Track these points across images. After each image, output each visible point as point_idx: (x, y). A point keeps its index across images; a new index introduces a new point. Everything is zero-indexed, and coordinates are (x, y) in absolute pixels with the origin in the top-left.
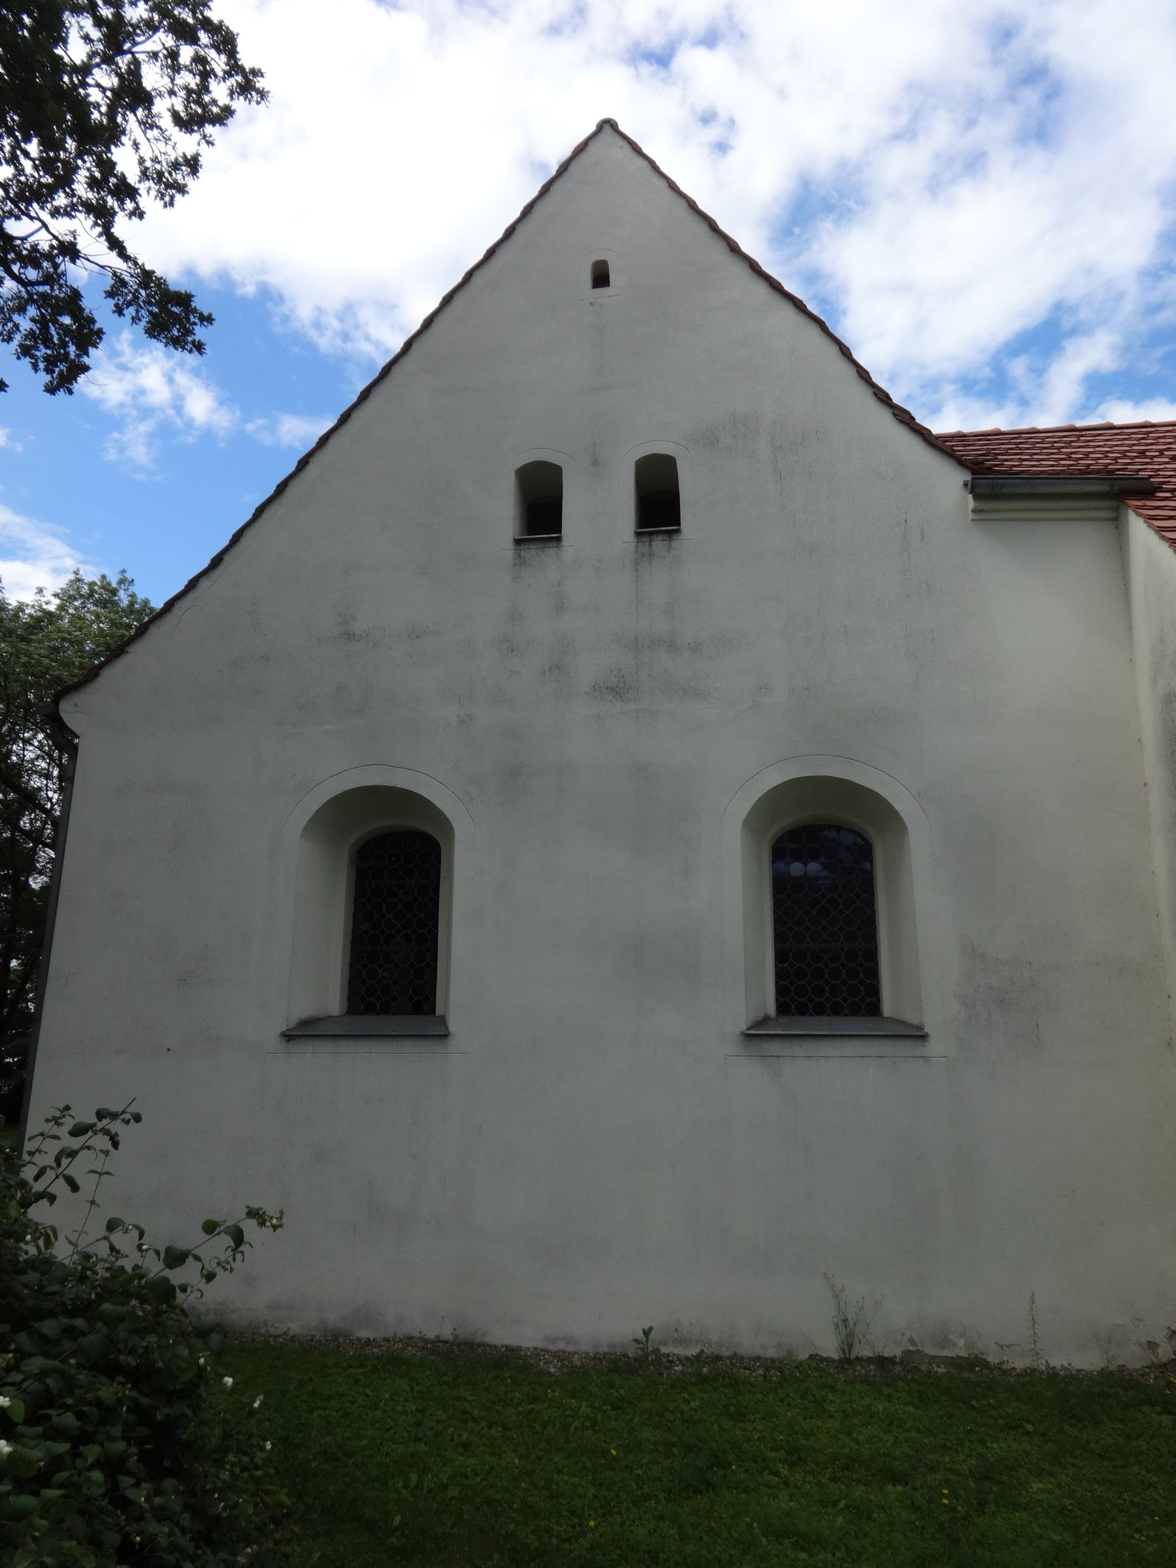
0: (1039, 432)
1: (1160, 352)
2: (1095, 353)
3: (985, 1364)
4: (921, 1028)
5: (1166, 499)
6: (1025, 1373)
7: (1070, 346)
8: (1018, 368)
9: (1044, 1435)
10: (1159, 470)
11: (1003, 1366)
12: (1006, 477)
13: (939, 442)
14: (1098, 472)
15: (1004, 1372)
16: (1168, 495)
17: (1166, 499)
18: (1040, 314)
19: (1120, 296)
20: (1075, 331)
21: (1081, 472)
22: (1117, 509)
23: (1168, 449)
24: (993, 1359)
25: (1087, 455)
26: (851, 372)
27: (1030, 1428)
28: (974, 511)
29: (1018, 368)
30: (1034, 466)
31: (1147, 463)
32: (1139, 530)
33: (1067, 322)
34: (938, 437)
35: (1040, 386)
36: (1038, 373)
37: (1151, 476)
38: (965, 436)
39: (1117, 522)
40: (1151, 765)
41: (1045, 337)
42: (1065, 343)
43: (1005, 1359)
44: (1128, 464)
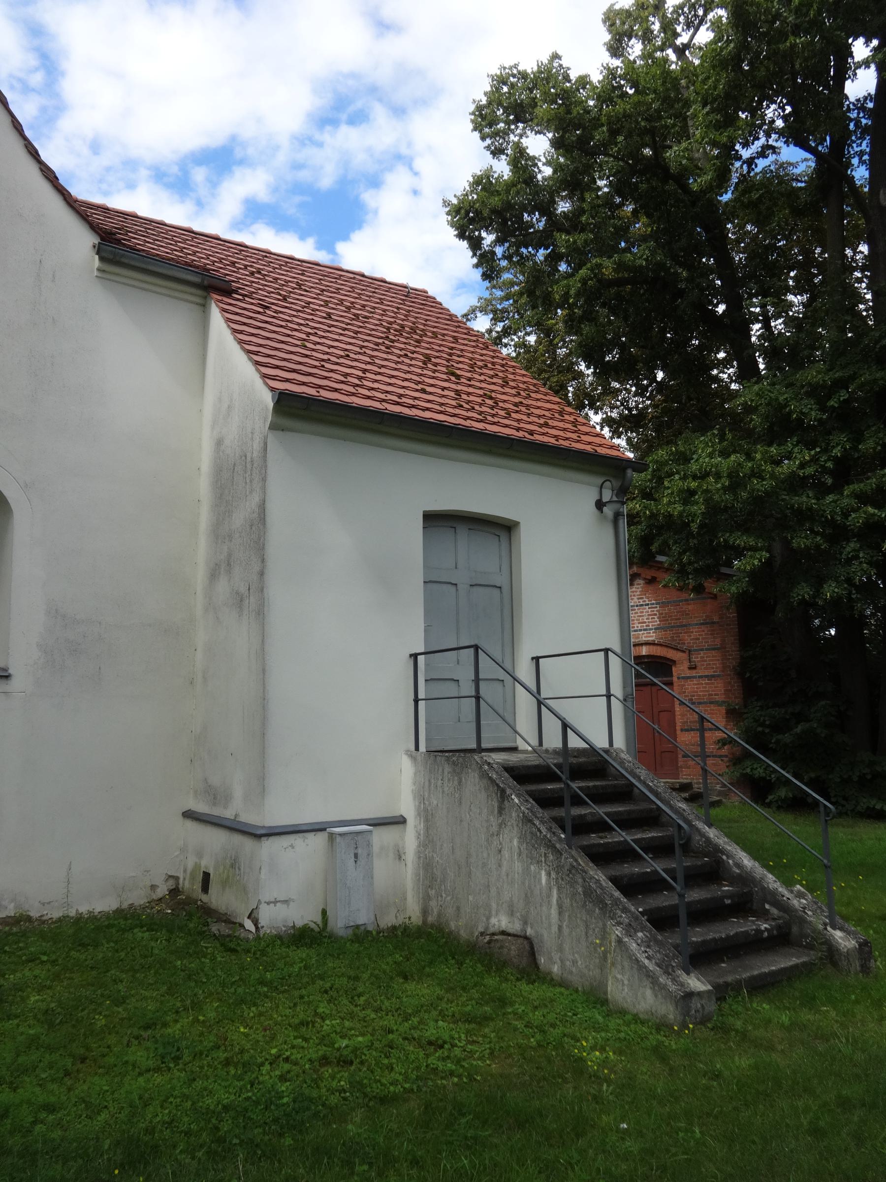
0: (165, 225)
1: (297, 199)
2: (251, 183)
3: (29, 919)
4: (6, 670)
5: (238, 300)
6: (59, 920)
7: (238, 172)
8: (199, 175)
9: (54, 961)
10: (240, 278)
11: (44, 918)
12: (123, 246)
13: (76, 205)
14: (197, 267)
15: (44, 922)
16: (240, 297)
17: (238, 300)
18: (217, 140)
19: (277, 148)
20: (242, 162)
21: (186, 264)
22: (205, 298)
23: (251, 266)
24: (34, 914)
25: (195, 253)
26: (7, 120)
27: (45, 958)
28: (98, 270)
29: (199, 175)
30: (153, 249)
31: (234, 272)
32: (216, 317)
33: (238, 153)
34: (76, 201)
35: (213, 195)
36: (214, 184)
37: (233, 281)
38: (108, 209)
39: (204, 307)
40: (204, 487)
41: (222, 159)
42: (234, 168)
43: (45, 912)
44: (221, 268)
